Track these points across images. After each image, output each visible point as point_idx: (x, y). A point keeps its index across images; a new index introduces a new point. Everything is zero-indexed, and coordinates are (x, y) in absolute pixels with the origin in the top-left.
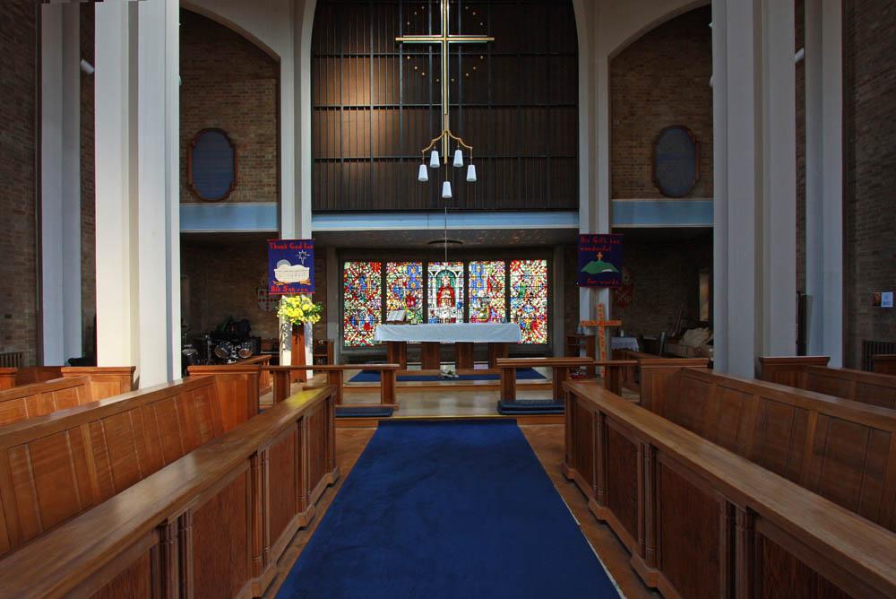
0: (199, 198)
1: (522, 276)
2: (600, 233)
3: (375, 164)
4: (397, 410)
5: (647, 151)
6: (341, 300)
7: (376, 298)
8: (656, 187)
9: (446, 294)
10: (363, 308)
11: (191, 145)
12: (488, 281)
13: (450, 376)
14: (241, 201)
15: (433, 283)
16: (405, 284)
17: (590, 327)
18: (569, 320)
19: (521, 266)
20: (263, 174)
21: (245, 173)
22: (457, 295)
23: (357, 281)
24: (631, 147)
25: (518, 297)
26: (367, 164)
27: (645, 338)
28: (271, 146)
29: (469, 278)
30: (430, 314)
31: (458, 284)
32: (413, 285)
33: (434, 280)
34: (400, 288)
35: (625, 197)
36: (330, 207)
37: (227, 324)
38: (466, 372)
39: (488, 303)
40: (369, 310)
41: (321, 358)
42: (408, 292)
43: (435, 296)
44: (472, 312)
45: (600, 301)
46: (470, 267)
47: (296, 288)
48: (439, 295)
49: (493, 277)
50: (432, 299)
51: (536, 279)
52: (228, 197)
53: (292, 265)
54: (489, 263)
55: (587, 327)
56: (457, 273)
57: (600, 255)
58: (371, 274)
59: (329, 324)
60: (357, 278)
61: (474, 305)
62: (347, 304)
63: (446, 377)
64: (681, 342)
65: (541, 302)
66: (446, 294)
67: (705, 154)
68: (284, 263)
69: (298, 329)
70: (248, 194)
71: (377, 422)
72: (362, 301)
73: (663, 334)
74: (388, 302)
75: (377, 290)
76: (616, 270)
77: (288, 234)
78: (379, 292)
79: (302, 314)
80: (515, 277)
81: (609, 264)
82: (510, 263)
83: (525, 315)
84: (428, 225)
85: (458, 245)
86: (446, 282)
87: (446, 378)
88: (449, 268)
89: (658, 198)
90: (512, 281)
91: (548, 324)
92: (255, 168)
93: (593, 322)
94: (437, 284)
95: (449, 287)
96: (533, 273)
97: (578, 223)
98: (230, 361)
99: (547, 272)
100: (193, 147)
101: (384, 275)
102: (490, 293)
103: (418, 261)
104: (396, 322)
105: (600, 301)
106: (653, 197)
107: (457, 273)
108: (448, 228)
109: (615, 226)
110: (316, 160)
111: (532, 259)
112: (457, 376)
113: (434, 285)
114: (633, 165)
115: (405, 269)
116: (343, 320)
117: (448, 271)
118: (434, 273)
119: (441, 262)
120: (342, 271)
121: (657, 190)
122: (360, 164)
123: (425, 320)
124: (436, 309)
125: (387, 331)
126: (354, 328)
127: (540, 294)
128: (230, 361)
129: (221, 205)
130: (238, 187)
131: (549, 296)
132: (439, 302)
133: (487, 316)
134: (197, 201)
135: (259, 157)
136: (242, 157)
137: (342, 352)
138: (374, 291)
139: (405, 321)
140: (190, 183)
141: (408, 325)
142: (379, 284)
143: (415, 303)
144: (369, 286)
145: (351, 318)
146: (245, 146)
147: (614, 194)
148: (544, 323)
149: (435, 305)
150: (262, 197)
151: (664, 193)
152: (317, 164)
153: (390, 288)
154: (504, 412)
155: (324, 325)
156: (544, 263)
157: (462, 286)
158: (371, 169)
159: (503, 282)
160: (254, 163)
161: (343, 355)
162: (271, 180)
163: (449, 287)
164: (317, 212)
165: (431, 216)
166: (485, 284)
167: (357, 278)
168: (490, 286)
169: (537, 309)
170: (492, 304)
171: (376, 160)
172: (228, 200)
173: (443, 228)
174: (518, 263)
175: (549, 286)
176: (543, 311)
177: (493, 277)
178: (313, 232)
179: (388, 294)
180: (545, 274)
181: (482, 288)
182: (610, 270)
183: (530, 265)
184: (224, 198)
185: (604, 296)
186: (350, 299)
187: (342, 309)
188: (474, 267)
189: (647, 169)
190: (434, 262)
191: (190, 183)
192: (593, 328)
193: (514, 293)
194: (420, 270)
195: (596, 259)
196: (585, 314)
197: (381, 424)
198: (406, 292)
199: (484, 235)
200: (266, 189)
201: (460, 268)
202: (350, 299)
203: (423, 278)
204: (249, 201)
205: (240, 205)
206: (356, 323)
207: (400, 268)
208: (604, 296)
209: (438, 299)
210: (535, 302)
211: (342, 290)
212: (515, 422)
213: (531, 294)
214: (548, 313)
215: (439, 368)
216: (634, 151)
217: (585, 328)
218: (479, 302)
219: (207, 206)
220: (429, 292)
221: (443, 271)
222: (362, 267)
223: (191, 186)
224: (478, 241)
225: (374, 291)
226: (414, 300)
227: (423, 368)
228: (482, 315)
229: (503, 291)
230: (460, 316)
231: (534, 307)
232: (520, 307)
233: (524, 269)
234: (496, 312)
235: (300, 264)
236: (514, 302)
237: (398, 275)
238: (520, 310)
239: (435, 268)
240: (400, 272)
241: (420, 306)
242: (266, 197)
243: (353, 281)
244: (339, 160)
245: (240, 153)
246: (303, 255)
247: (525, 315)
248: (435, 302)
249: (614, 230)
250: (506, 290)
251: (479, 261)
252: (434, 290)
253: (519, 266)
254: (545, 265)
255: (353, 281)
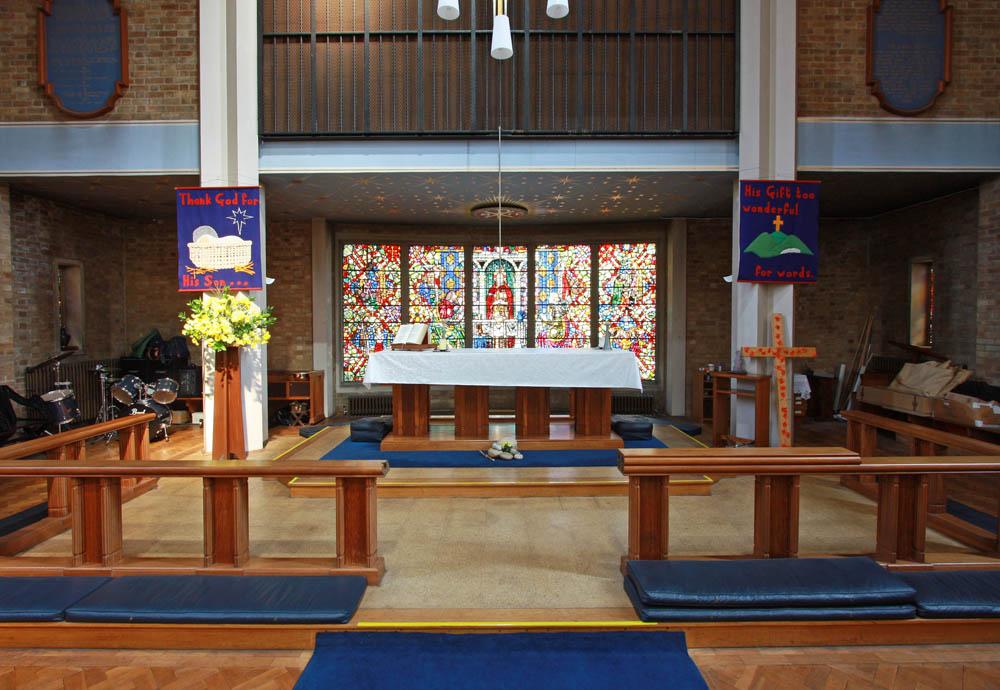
0: (61, 111)
1: (616, 270)
2: (777, 179)
3: (372, 46)
4: (377, 584)
5: (858, 26)
6: (338, 307)
7: (393, 303)
8: (873, 94)
9: (501, 297)
10: (372, 319)
11: (42, 10)
12: (564, 278)
13: (508, 456)
14: (133, 117)
15: (480, 280)
16: (437, 281)
17: (759, 358)
18: (693, 342)
19: (616, 254)
20: (173, 67)
21: (143, 65)
22: (517, 300)
23: (363, 277)
24: (830, 18)
25: (611, 304)
26: (355, 45)
27: (815, 374)
28: (186, 14)
29: (535, 272)
30: (475, 330)
31: (519, 282)
32: (450, 284)
33: (483, 276)
34: (429, 288)
35: (818, 114)
36: (293, 129)
37: (148, 345)
38: (536, 444)
39: (565, 313)
40: (382, 322)
41: (300, 402)
42: (443, 295)
43: (483, 301)
44: (539, 328)
45: (776, 310)
46: (537, 255)
47: (229, 280)
48: (490, 300)
49: (571, 270)
50: (479, 310)
51: (639, 275)
52: (111, 109)
53: (220, 235)
54: (566, 249)
55: (753, 358)
56: (518, 264)
57: (778, 222)
58: (387, 266)
59: (315, 344)
60: (364, 270)
61: (543, 316)
62: (348, 313)
63: (498, 458)
64: (894, 384)
65: (647, 310)
66: (501, 297)
67: (960, 33)
68: (209, 233)
69: (229, 358)
70: (148, 103)
71: (312, 636)
72: (371, 309)
73: (843, 367)
74: (411, 309)
75: (395, 290)
76: (808, 252)
77: (213, 177)
78: (398, 294)
79: (229, 330)
80: (605, 269)
81: (794, 238)
82: (599, 250)
83: (620, 333)
84: (468, 164)
85: (519, 213)
86: (500, 279)
87: (499, 462)
88: (506, 256)
89: (875, 115)
90: (600, 278)
91: (657, 348)
92: (160, 54)
93: (765, 349)
94: (487, 281)
95: (503, 288)
96: (635, 266)
97: (737, 162)
98: (135, 411)
99: (656, 263)
100: (47, 15)
101: (405, 267)
102: (568, 298)
103: (457, 245)
104: (409, 347)
105: (776, 310)
106: (867, 115)
107: (518, 264)
108: (505, 169)
109: (800, 169)
110: (265, 39)
111: (634, 243)
112: (519, 456)
113: (482, 284)
114: (832, 53)
115: (438, 256)
116: (341, 337)
117: (504, 260)
118: (482, 264)
119: (492, 246)
120: (338, 260)
121: (874, 101)
122: (345, 46)
123: (468, 342)
124: (485, 321)
125: (389, 363)
126: (359, 352)
127: (644, 299)
128: (135, 411)
129: (99, 125)
130: (129, 91)
131: (661, 304)
132: (489, 311)
133: (563, 333)
134: (56, 118)
135: (167, 34)
136: (136, 34)
137: (339, 390)
138: (391, 292)
139: (425, 344)
140: (43, 82)
141: (429, 353)
142: (397, 280)
143: (453, 313)
144: (383, 284)
145: (354, 335)
146: (141, 14)
147: (801, 111)
148: (650, 346)
149: (484, 316)
150: (172, 110)
151: (889, 109)
152: (267, 47)
153: (415, 288)
154: (652, 613)
155: (309, 348)
156: (652, 249)
157: (525, 285)
158: (366, 58)
159: (587, 280)
160: (158, 45)
161: (341, 395)
162: (188, 77)
163: (503, 288)
164: (269, 136)
165: (472, 143)
166: (560, 283)
167: (364, 270)
168: (568, 288)
169: (639, 324)
170: (570, 315)
171: (374, 37)
172: (113, 113)
173: (494, 169)
174: (611, 249)
175: (660, 287)
176: (649, 327)
177: (571, 270)
178: (260, 175)
179: (412, 297)
180: (653, 267)
181: (555, 288)
182: (797, 251)
183: (630, 252)
184: (103, 113)
185: (784, 299)
186: (353, 306)
187: (339, 322)
188: (543, 255)
189: (858, 60)
190: (482, 246)
191: (43, 82)
192: (762, 361)
193: (604, 298)
194: (461, 259)
195: (771, 229)
196: (746, 332)
197: (324, 642)
198: (439, 295)
199: (561, 190)
200: (180, 94)
201: (521, 255)
202: (353, 306)
203: (465, 271)
204: (148, 117)
205: (134, 124)
206: (362, 344)
207: (429, 256)
208: (784, 299)
209: (488, 306)
210: (636, 312)
211: (338, 289)
212: (678, 642)
213: (631, 299)
214: (657, 330)
215: (485, 434)
216: (837, 25)
217: (747, 360)
218: (550, 311)
219: (74, 126)
220: (475, 294)
221: (495, 261)
222: (372, 253)
223: (44, 87)
224: (555, 204)
225: (391, 292)
226: (452, 307)
227: (458, 434)
228: (554, 332)
229: (588, 294)
230: (520, 333)
231: (635, 320)
232: (614, 320)
233: (620, 259)
234: (577, 327)
235: (235, 233)
236: (604, 312)
237: (427, 266)
238: (614, 325)
239: (482, 255)
240: (432, 262)
241: (461, 316)
242: (179, 109)
243: (358, 276)
244: (307, 38)
245: (132, 25)
246: (240, 217)
247: (620, 333)
248: (483, 310)
249: (800, 174)
250: (471, 323)
251: (552, 245)
252: (483, 293)
253: (612, 253)
254: (654, 252)
255: (358, 276)
